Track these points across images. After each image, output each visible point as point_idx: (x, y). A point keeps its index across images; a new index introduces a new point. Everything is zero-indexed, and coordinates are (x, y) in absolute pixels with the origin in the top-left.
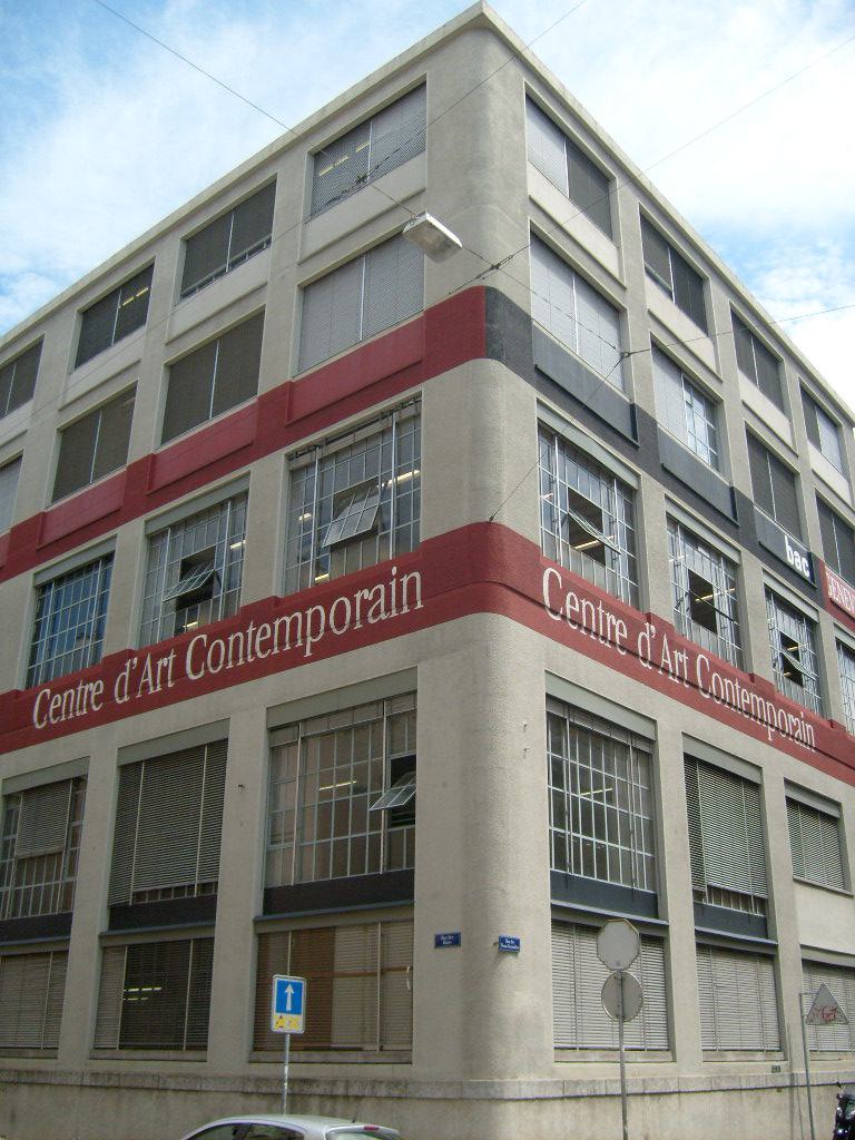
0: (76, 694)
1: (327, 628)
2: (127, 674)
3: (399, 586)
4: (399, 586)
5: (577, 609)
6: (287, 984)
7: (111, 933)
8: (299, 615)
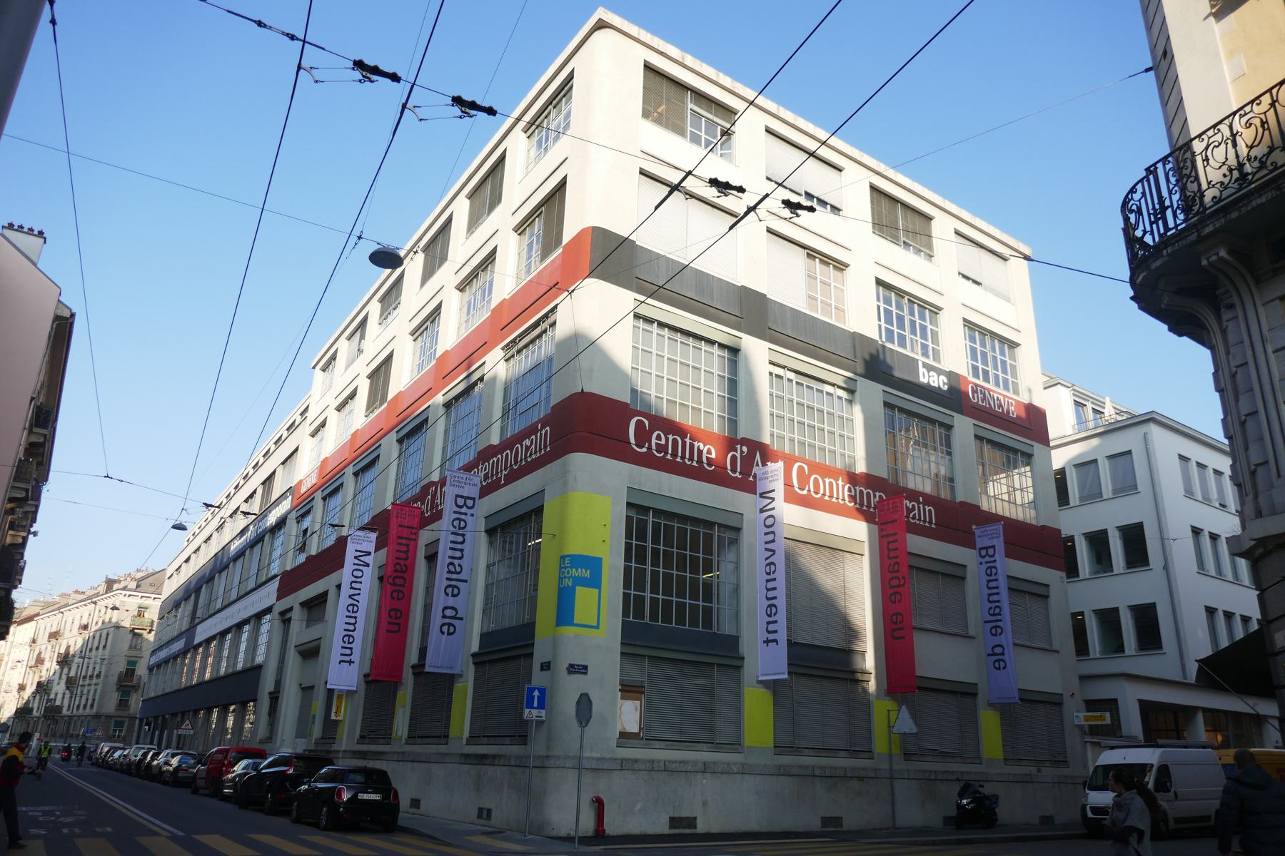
0: (502, 458)
1: (511, 465)
2: (430, 497)
3: (541, 434)
4: (541, 434)
5: (663, 442)
6: (169, 835)
7: (481, 652)
8: (500, 456)
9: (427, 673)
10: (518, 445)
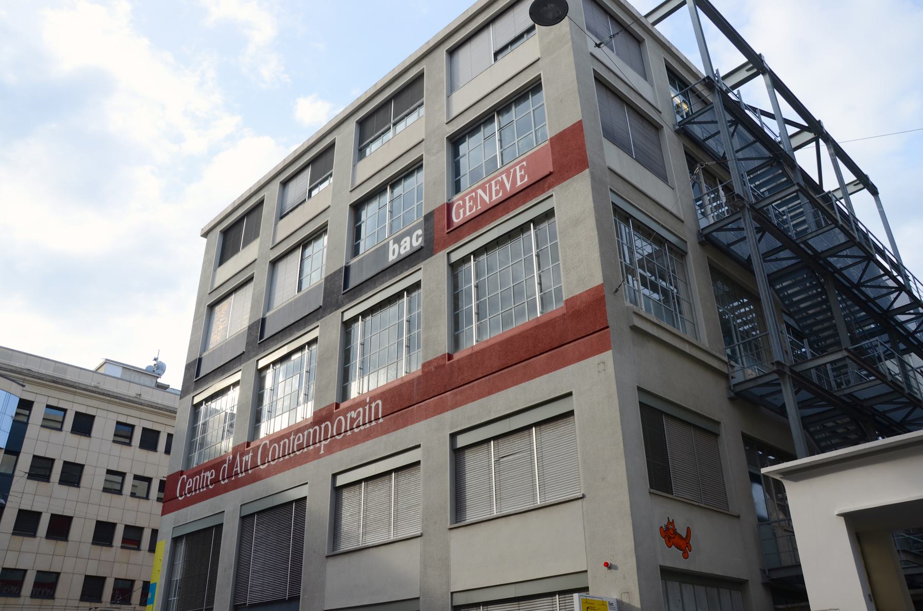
2: (226, 465)
3: (370, 408)
4: (370, 408)
9: (868, 305)
10: (276, 445)
